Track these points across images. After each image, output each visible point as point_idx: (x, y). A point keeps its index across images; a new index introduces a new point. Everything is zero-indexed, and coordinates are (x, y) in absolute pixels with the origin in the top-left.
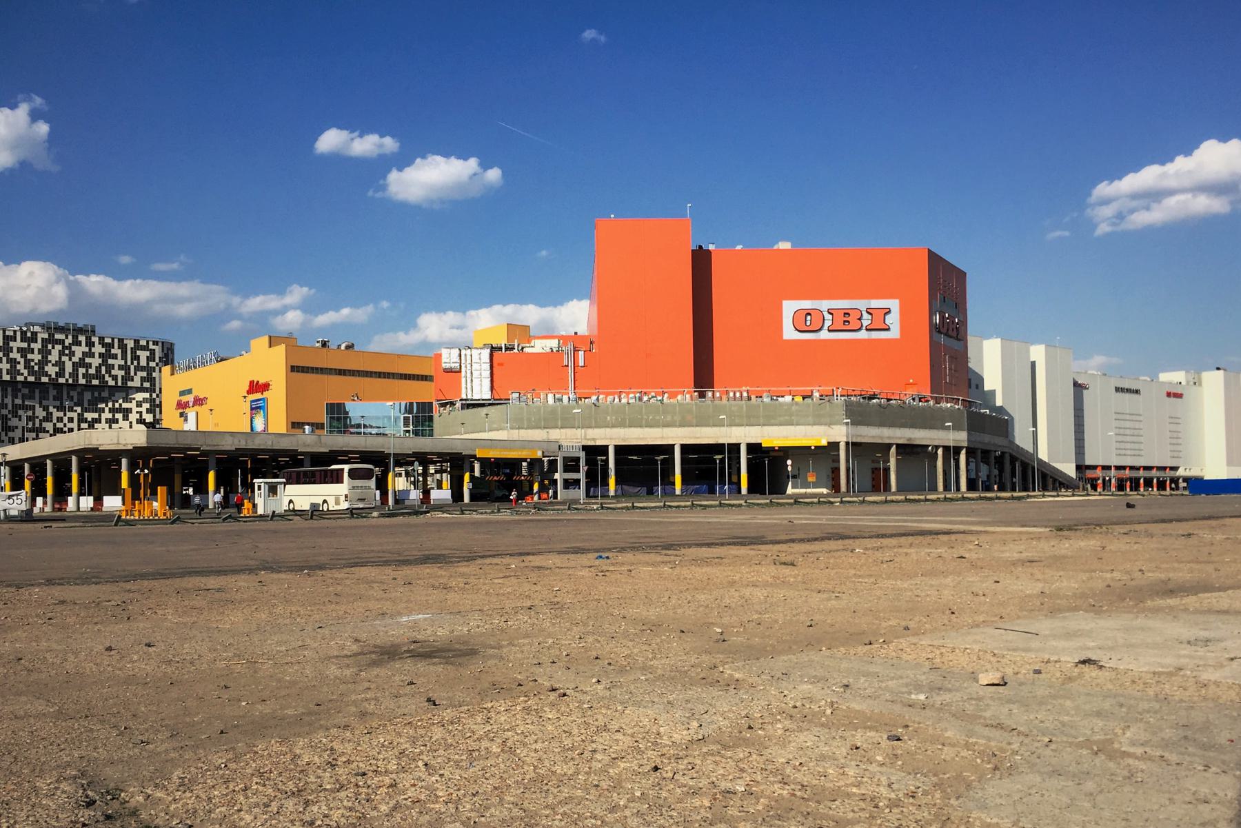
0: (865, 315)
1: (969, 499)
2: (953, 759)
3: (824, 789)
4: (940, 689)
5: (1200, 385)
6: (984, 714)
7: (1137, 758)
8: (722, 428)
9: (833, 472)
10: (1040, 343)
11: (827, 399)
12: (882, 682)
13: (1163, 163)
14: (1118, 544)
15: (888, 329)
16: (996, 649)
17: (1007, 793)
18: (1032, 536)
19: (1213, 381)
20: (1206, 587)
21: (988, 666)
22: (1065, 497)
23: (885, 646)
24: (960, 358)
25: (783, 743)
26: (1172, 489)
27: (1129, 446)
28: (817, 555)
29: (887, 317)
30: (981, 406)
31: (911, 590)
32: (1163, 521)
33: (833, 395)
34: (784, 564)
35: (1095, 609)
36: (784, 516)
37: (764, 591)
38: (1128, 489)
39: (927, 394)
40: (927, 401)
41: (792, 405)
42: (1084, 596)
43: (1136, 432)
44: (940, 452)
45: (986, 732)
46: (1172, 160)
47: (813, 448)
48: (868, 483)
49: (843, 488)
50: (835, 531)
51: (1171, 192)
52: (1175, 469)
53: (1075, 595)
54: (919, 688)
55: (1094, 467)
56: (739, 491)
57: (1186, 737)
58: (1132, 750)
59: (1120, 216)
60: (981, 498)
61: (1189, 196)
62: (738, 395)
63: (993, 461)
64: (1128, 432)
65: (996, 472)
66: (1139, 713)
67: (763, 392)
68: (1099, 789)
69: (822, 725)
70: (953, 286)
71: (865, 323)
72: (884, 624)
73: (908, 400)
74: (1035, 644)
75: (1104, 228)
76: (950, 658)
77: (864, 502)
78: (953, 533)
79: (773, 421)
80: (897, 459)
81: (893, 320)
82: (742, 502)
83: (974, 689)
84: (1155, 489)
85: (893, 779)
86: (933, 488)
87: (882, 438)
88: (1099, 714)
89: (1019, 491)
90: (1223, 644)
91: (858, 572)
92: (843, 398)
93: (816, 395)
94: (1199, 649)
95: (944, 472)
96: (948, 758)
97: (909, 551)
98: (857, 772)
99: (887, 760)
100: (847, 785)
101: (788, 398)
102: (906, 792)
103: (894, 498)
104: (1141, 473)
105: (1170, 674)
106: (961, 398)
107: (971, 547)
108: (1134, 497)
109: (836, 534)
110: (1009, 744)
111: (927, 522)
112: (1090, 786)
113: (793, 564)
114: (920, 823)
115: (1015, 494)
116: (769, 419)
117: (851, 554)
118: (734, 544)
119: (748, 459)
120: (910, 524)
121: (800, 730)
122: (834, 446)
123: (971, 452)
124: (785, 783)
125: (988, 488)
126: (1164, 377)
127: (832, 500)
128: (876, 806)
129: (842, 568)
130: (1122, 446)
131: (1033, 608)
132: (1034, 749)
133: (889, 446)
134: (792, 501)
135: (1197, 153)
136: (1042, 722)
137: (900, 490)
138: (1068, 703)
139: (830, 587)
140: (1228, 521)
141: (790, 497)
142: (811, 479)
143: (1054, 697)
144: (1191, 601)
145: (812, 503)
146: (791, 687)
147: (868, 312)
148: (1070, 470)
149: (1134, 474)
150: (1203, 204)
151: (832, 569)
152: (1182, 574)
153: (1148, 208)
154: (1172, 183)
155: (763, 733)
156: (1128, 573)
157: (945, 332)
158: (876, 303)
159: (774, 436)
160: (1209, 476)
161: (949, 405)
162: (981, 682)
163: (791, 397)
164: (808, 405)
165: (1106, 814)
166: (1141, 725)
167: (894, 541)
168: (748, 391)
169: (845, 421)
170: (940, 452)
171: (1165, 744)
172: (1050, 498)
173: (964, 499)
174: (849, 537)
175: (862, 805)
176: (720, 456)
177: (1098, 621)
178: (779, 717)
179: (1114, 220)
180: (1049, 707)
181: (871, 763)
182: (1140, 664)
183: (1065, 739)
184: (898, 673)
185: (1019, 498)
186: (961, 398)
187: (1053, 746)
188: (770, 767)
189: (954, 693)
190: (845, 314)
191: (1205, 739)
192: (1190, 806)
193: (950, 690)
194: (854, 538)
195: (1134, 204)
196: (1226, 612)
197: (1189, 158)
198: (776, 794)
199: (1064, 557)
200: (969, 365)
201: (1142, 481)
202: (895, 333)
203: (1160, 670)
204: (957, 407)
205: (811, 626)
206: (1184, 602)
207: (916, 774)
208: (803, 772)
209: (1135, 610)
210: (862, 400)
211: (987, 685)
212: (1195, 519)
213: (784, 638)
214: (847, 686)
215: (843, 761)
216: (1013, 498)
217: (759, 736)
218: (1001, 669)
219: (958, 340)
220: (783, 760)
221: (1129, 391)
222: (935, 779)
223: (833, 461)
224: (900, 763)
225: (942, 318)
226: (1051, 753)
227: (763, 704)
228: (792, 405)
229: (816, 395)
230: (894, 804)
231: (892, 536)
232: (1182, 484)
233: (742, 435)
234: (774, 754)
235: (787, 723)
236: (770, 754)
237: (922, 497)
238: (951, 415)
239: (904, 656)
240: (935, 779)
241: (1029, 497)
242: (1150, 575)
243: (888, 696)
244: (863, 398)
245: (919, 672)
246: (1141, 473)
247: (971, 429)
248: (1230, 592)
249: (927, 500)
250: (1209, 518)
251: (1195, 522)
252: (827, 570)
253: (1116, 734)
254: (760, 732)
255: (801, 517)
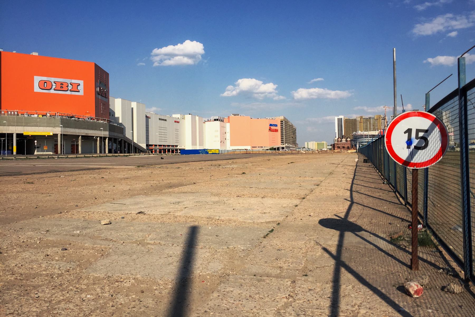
0: (70, 85)
1: (108, 156)
2: (87, 254)
3: (31, 274)
4: (86, 228)
5: (184, 119)
6: (101, 236)
7: (152, 245)
8: (5, 127)
9: (55, 146)
10: (135, 101)
11: (53, 117)
12: (63, 228)
13: (174, 46)
14: (157, 171)
15: (79, 92)
16: (110, 211)
17: (104, 264)
18: (129, 169)
19: (188, 118)
20: (182, 185)
21: (106, 217)
22: (142, 155)
23: (67, 214)
24: (107, 105)
25: (15, 257)
26: (176, 153)
27: (163, 138)
28: (44, 179)
29: (78, 87)
30: (114, 123)
31: (81, 191)
32: (172, 163)
33: (56, 115)
34: (29, 183)
35: (146, 194)
36: (32, 163)
37: (17, 194)
38: (163, 153)
39: (94, 117)
40: (94, 120)
41: (38, 118)
42: (143, 190)
43: (165, 134)
44: (98, 139)
45: (101, 242)
46: (177, 45)
47: (46, 136)
48: (70, 150)
49: (59, 152)
50: (53, 169)
51: (176, 55)
52: (177, 146)
53: (140, 190)
54: (77, 228)
55: (152, 145)
56: (12, 153)
57: (168, 235)
58: (150, 242)
59: (161, 61)
60: (113, 156)
61: (182, 57)
62: (13, 113)
63: (118, 142)
64: (163, 133)
65: (119, 146)
66: (154, 229)
67: (24, 112)
68: (137, 257)
69: (35, 248)
70: (104, 78)
71: (70, 88)
72: (68, 205)
73: (87, 119)
74: (124, 208)
75: (156, 64)
76: (92, 216)
77: (67, 157)
78: (101, 169)
79: (28, 125)
80: (82, 141)
81: (81, 88)
82: (13, 158)
83: (99, 226)
84: (171, 153)
85: (61, 265)
86: (96, 152)
87: (76, 133)
88: (141, 231)
89: (127, 153)
90: (183, 203)
91: (60, 185)
92: (60, 117)
93: (48, 115)
94: (176, 205)
95: (100, 146)
96: (85, 254)
97: (83, 176)
98: (46, 265)
99: (60, 258)
100: (41, 271)
101: (36, 116)
102: (65, 270)
103: (80, 156)
104: (167, 147)
105: (166, 215)
106: (107, 119)
107: (107, 174)
108: (163, 155)
109: (54, 170)
110: (109, 245)
111: (93, 165)
112: (134, 257)
113: (32, 183)
114: (69, 281)
115: (125, 154)
116: (27, 124)
117: (59, 178)
118: (6, 175)
119: (17, 140)
120: (86, 166)
121: (24, 251)
122: (56, 135)
123: (110, 139)
124: (13, 275)
125: (116, 152)
126: (174, 116)
127: (54, 157)
128: (52, 278)
129: (54, 184)
130: (161, 138)
131: (125, 195)
132: (117, 246)
133: (79, 136)
134: (37, 157)
135: (184, 43)
136: (122, 236)
137: (82, 153)
138: (132, 228)
139: (47, 192)
140: (191, 163)
141: (36, 156)
142: (45, 148)
143: (127, 226)
144: (176, 190)
145: (45, 158)
146: (23, 234)
147: (71, 84)
148: (144, 146)
149: (165, 148)
150: (186, 61)
151: (50, 184)
152: (175, 181)
153: (170, 59)
154: (177, 52)
155: (7, 254)
156: (159, 181)
157: (101, 94)
158: (74, 81)
159: (29, 131)
160: (187, 148)
161: (102, 122)
162: (102, 224)
163: (37, 115)
164: (45, 119)
165: (138, 266)
166: (154, 233)
167: (77, 173)
168: (17, 112)
169: (60, 126)
170: (98, 139)
171: (161, 239)
172: (137, 156)
173: (107, 156)
174: (59, 171)
175: (46, 278)
176: (4, 139)
177: (146, 198)
178: (15, 247)
179: (159, 62)
180: (125, 230)
181: (53, 261)
182: (157, 212)
183: (129, 241)
184: (70, 223)
185: (127, 156)
186: (107, 119)
187: (124, 244)
188: (7, 269)
189: (91, 229)
190: (61, 84)
191: (173, 235)
192: (166, 259)
193: (89, 228)
194: (61, 171)
195: (166, 57)
196: (186, 193)
197: (182, 45)
198: (8, 280)
199: (139, 176)
200: (110, 107)
201: (167, 150)
202: (81, 93)
203: (163, 213)
204: (105, 122)
205: (36, 208)
206: (174, 190)
207: (71, 262)
208: (22, 269)
209: (159, 194)
210: (67, 118)
211: (104, 224)
212: (181, 163)
213: (23, 214)
214: (48, 231)
215: (41, 261)
216: (124, 156)
217: (5, 256)
218: (110, 218)
219: (106, 98)
220: (14, 265)
221: (163, 120)
222: (78, 263)
223: (55, 141)
224: (65, 259)
225: (100, 89)
226: (123, 247)
227: (8, 242)
228: (38, 118)
229: (48, 115)
230: (60, 275)
231: (77, 170)
232: (179, 151)
233: (15, 130)
234: (10, 263)
235: (18, 249)
236: (8, 263)
237: (91, 156)
238: (102, 125)
239: (74, 217)
240: (78, 263)
241: (130, 155)
242: (165, 181)
243: (65, 233)
244: (68, 117)
245: (78, 222)
246: (167, 147)
247: (110, 131)
248: (188, 186)
249: (93, 157)
250: (185, 162)
251: (181, 164)
252: (47, 185)
253: (146, 237)
254: (5, 254)
255: (39, 164)
